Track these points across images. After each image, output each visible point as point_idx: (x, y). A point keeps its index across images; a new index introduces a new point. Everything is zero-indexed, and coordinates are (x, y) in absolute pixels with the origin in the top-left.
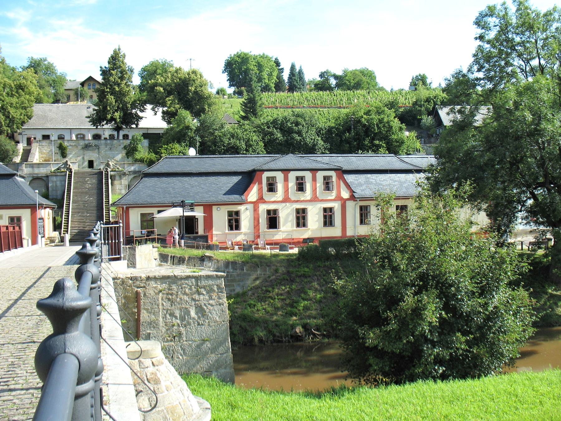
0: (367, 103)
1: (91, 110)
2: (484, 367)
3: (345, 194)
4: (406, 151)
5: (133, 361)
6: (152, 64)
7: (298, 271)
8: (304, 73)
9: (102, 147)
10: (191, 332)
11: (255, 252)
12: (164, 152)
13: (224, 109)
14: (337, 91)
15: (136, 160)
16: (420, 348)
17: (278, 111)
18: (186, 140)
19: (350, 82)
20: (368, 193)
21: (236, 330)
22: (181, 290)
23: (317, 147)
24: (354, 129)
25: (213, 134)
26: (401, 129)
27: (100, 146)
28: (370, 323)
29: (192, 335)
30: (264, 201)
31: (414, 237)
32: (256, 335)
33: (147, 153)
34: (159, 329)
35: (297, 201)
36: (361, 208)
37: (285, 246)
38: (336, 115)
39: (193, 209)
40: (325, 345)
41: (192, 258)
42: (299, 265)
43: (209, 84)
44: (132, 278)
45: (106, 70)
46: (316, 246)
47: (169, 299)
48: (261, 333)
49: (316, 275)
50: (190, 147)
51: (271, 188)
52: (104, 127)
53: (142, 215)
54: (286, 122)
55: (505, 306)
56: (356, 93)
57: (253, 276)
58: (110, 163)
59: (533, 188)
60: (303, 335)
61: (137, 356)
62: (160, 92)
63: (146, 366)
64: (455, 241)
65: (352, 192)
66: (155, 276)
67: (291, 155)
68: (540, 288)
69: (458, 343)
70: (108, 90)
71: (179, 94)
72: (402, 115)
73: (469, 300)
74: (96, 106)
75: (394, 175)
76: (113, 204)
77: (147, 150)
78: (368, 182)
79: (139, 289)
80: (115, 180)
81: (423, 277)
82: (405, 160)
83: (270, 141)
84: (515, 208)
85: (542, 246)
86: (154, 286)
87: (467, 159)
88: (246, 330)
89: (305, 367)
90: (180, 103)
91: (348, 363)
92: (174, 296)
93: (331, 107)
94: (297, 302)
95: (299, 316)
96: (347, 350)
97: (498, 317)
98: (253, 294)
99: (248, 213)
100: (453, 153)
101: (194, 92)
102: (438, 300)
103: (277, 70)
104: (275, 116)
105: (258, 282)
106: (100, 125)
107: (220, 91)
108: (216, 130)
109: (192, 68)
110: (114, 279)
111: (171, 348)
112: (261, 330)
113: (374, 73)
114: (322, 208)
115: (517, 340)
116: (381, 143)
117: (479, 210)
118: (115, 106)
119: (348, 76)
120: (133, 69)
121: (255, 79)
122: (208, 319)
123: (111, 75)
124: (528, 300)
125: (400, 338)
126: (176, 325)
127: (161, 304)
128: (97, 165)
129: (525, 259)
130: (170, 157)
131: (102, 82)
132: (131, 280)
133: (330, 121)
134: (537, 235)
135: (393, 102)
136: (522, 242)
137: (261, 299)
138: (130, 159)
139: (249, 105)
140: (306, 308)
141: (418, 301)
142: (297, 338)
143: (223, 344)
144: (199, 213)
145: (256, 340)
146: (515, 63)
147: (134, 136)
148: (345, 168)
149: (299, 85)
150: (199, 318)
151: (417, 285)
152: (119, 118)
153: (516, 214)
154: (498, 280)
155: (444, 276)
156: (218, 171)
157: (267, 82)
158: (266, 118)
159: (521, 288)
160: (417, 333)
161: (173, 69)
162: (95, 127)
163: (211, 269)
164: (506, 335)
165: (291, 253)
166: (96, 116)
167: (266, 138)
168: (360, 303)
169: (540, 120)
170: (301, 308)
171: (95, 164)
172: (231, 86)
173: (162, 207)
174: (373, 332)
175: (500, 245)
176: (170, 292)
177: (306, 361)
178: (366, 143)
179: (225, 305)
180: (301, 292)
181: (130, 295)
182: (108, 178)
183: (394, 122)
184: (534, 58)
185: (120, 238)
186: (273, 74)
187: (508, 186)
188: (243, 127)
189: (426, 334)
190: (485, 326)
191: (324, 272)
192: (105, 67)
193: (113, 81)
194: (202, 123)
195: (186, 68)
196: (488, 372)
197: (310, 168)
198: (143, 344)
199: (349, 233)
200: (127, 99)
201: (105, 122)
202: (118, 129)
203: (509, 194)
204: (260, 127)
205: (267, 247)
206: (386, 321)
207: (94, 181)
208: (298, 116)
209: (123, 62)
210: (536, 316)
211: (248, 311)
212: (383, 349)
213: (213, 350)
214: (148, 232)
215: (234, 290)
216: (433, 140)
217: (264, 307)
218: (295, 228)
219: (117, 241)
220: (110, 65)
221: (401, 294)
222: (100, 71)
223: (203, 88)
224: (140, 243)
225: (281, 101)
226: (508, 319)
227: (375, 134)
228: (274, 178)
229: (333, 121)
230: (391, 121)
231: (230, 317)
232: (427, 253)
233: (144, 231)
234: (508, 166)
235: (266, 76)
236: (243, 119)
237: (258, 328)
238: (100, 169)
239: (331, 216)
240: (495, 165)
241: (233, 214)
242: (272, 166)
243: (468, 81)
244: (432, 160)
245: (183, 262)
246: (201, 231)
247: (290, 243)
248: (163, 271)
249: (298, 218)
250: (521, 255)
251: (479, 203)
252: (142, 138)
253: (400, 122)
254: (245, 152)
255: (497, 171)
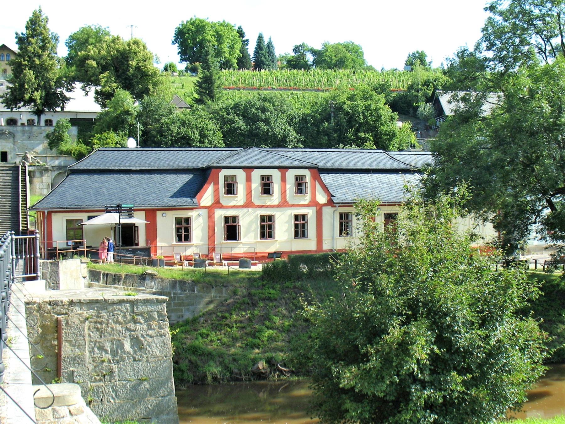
0: (352, 86)
1: (4, 87)
2: (483, 414)
3: (322, 199)
4: (398, 146)
5: (46, 410)
6: (83, 31)
7: (262, 293)
8: (274, 46)
9: (19, 135)
10: (125, 370)
11: (209, 269)
12: (97, 143)
13: (173, 90)
14: (315, 70)
15: (62, 153)
16: (408, 390)
17: (241, 93)
18: (124, 128)
19: (330, 59)
20: (349, 198)
21: (184, 365)
22: (112, 317)
23: (288, 140)
24: (334, 117)
25: (159, 120)
26: (392, 119)
27: (16, 134)
28: (347, 359)
29: (127, 373)
30: (220, 206)
31: (401, 254)
32: (209, 371)
33: (75, 144)
34: (85, 366)
35: (262, 206)
36: (341, 215)
37: (246, 261)
38: (312, 100)
39: (131, 214)
40: (294, 384)
41: (130, 276)
42: (264, 285)
43: (155, 57)
44: (50, 302)
45: (24, 38)
46: (284, 262)
47: (97, 329)
48: (214, 369)
49: (284, 298)
50: (129, 137)
51: (230, 189)
52: (20, 110)
53: (68, 222)
54: (251, 108)
55: (510, 339)
56: (338, 72)
57: (205, 298)
58: (28, 155)
59: (550, 195)
60: (266, 372)
61: (51, 403)
62: (92, 67)
63: (62, 416)
64: (451, 260)
65: (330, 196)
66: (80, 300)
67: (255, 149)
68: (556, 317)
69: (453, 384)
70: (26, 63)
71: (116, 70)
72: (394, 100)
73: (467, 332)
74: (11, 83)
75: (383, 175)
76: (32, 208)
77: (76, 140)
78: (349, 184)
79: (60, 317)
80: (34, 176)
81: (413, 305)
82: (397, 157)
83: (229, 131)
84: (528, 219)
85: (559, 265)
86: (79, 312)
87: (471, 158)
88: (197, 366)
89: (270, 411)
90: (117, 81)
91: (320, 407)
92: (104, 325)
93: (307, 90)
94: (260, 331)
95: (262, 348)
96: (318, 391)
97: (501, 353)
98: (206, 321)
99: (201, 220)
100: (454, 150)
101: (136, 67)
102: (429, 333)
103: (240, 41)
104: (237, 100)
105: (211, 306)
106: (16, 107)
107: (168, 67)
108: (163, 115)
109: (134, 37)
110: (27, 303)
111: (100, 390)
112: (215, 365)
113: (361, 49)
114: (293, 215)
115: (523, 381)
116: (367, 135)
117: (485, 220)
118: (34, 83)
119: (329, 51)
120: (58, 37)
121: (212, 52)
122: (146, 354)
123: (30, 43)
124: (538, 333)
125: (383, 378)
126: (106, 360)
127: (87, 335)
128: (11, 158)
129: (535, 283)
130: (104, 149)
131: (19, 53)
132: (50, 304)
133: (305, 106)
134: (552, 252)
135: (383, 85)
136: (536, 261)
137: (215, 328)
138: (54, 150)
139: (204, 85)
140: (271, 339)
141: (405, 333)
142: (260, 375)
143: (165, 384)
144: (139, 220)
145: (209, 378)
146: (533, 41)
147: (59, 121)
148: (322, 166)
149: (267, 61)
150: (135, 352)
151: (405, 314)
152: (40, 99)
153: (530, 227)
154: (502, 308)
155: (438, 302)
156: (164, 168)
157: (228, 56)
158: (226, 102)
159: (530, 319)
160: (403, 372)
161: (108, 38)
162: (9, 110)
163: (154, 290)
164: (510, 375)
165: (254, 270)
166: (11, 95)
167: (225, 127)
168: (334, 334)
169: (560, 112)
170: (265, 339)
171: (9, 157)
172: (182, 60)
173: (93, 212)
174: (349, 371)
175: (507, 264)
176: (98, 319)
177: (271, 404)
178: (349, 135)
179: (167, 336)
180: (265, 319)
181: (49, 323)
182: (25, 174)
183: (383, 110)
184: (557, 36)
185: (37, 252)
186: (236, 47)
187: (520, 192)
188: (196, 112)
189: (415, 372)
190: (486, 363)
191: (294, 295)
192: (22, 34)
193: (33, 51)
194: (145, 107)
195: (126, 37)
196: (489, 420)
197: (278, 165)
198: (57, 389)
199: (326, 246)
200: (49, 75)
201: (22, 103)
202: (39, 113)
203: (521, 202)
204: (218, 113)
205: (224, 262)
206: (366, 358)
207: (8, 178)
208: (265, 100)
209: (44, 28)
210: (548, 352)
211: (199, 342)
212: (361, 391)
213: (152, 391)
214: (76, 243)
215: (182, 317)
216: (431, 132)
217: (220, 337)
218: (259, 240)
219: (32, 256)
220: (28, 31)
221: (384, 324)
222: (16, 38)
223: (147, 62)
224: (65, 256)
225: (245, 81)
226: (514, 356)
227: (361, 125)
228: (233, 177)
229: (310, 107)
230: (380, 108)
231: (175, 352)
232: (417, 274)
233: (71, 243)
234: (520, 167)
235: (226, 50)
236: (197, 103)
237: (212, 363)
238: (15, 163)
239: (303, 226)
240: (504, 167)
241: (183, 221)
242: (232, 162)
243: (477, 60)
244: (429, 158)
245: (119, 281)
246: (142, 242)
247: (252, 258)
248: (91, 293)
249: (263, 227)
250: (532, 276)
251: (485, 212)
252: (70, 124)
253: (391, 110)
254: (198, 144)
255: (508, 173)
